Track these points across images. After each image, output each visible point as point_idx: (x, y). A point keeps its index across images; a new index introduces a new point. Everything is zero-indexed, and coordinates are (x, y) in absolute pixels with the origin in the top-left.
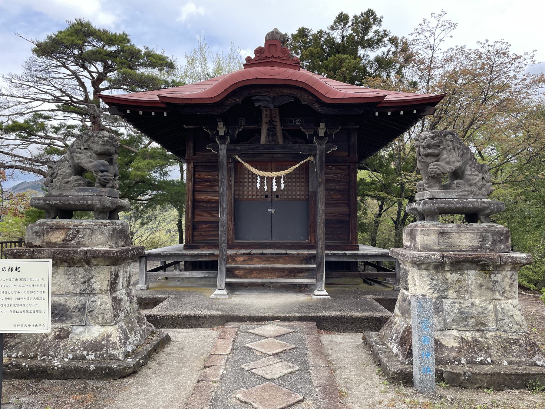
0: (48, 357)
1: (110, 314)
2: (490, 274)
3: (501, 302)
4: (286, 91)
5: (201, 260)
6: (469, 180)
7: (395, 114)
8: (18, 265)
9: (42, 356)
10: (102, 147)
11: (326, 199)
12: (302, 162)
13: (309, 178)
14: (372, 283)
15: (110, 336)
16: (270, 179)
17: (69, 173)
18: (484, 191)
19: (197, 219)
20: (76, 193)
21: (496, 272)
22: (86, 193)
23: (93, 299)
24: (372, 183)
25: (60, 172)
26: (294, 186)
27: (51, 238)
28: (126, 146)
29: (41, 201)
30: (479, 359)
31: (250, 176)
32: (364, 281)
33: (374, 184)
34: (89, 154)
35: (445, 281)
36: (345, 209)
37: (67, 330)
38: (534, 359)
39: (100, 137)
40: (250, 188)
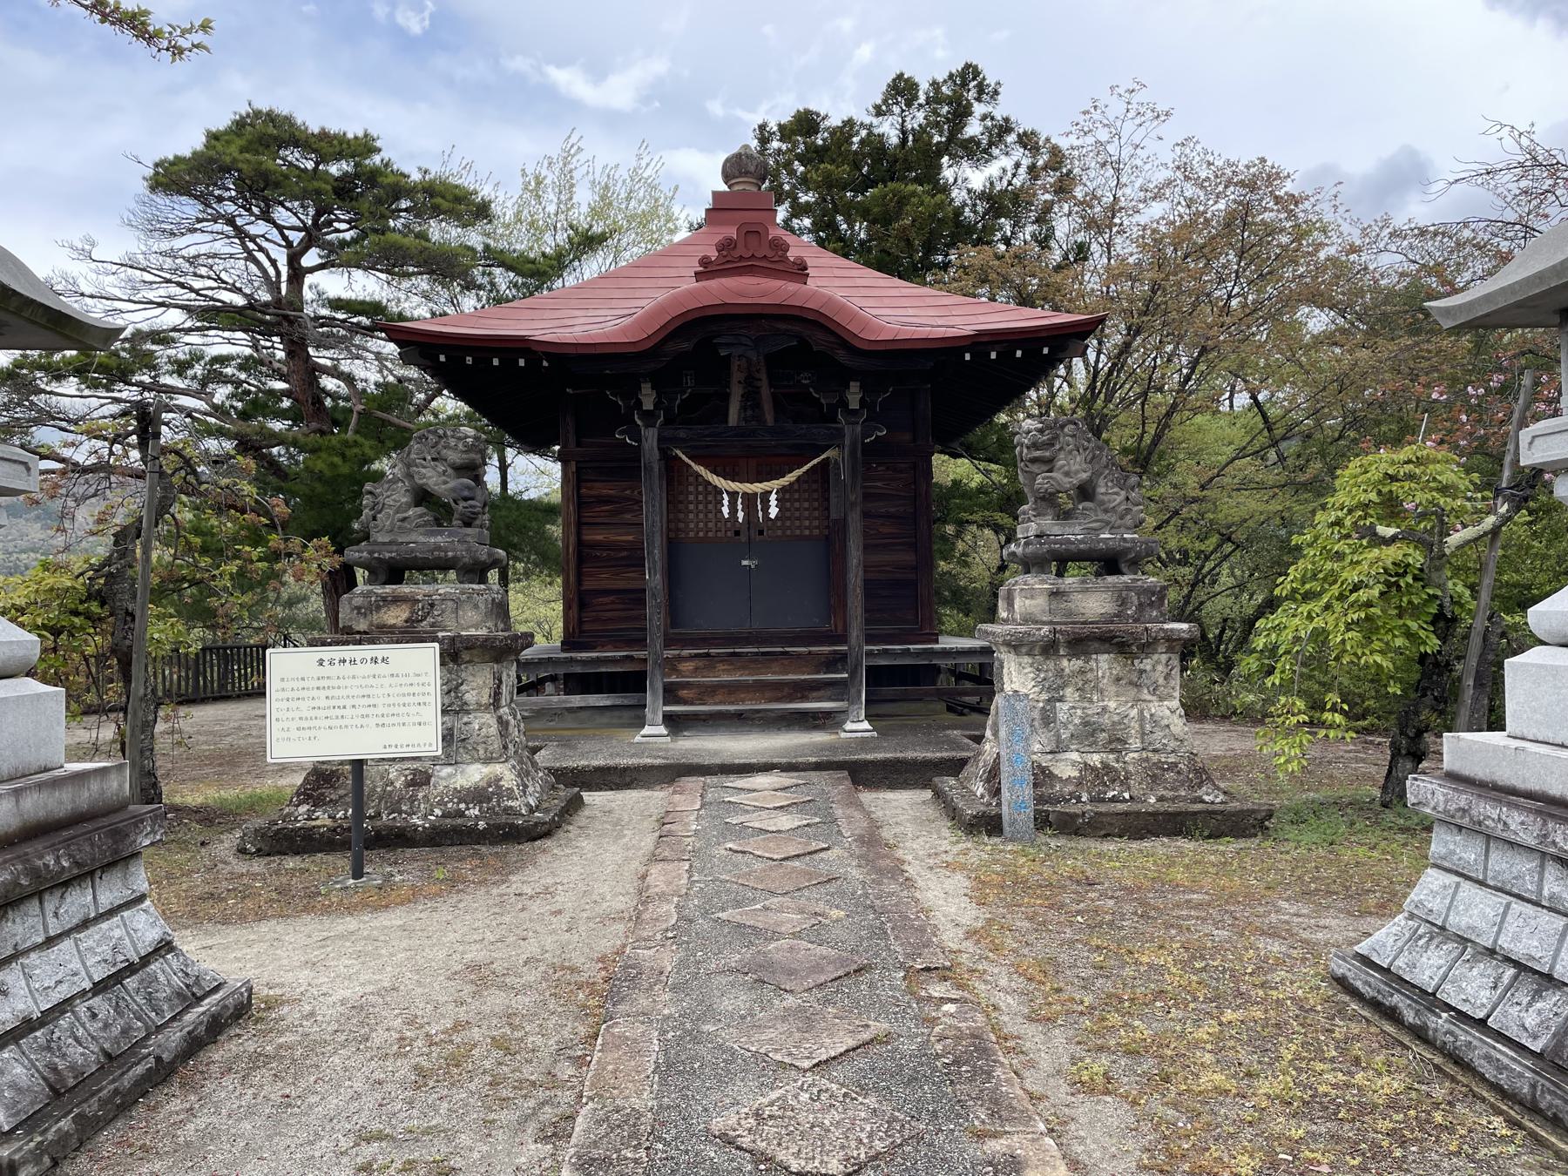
0: (400, 814)
1: (496, 745)
2: (1134, 659)
3: (1151, 705)
4: (782, 326)
5: (603, 670)
6: (1102, 503)
7: (1007, 355)
8: (385, 654)
9: (390, 814)
10: (464, 456)
11: (866, 535)
12: (815, 461)
13: (828, 490)
14: (966, 711)
15: (501, 779)
16: (749, 499)
17: (406, 503)
18: (1128, 520)
19: (588, 584)
20: (422, 539)
21: (1143, 656)
22: (439, 539)
23: (465, 719)
24: (981, 490)
25: (389, 501)
26: (797, 509)
27: (386, 617)
28: (379, 414)
29: (365, 554)
30: (1110, 794)
31: (700, 488)
32: (950, 709)
33: (986, 494)
34: (441, 468)
35: (1060, 673)
36: (908, 558)
37: (426, 772)
38: (1199, 793)
39: (459, 439)
40: (701, 516)
